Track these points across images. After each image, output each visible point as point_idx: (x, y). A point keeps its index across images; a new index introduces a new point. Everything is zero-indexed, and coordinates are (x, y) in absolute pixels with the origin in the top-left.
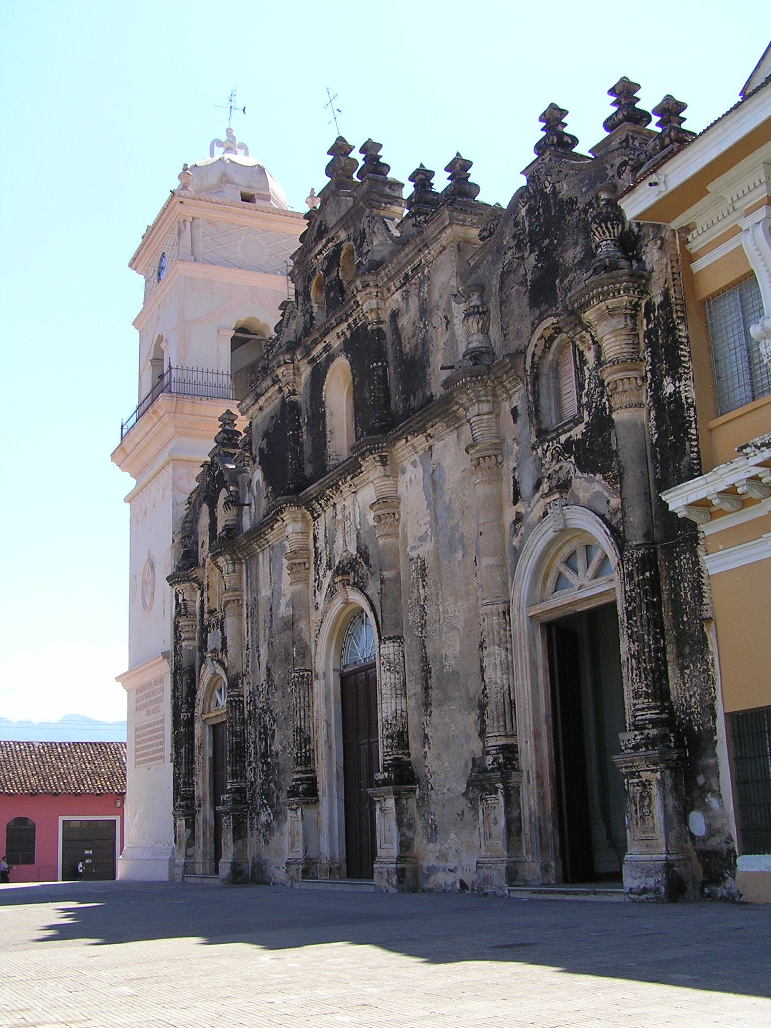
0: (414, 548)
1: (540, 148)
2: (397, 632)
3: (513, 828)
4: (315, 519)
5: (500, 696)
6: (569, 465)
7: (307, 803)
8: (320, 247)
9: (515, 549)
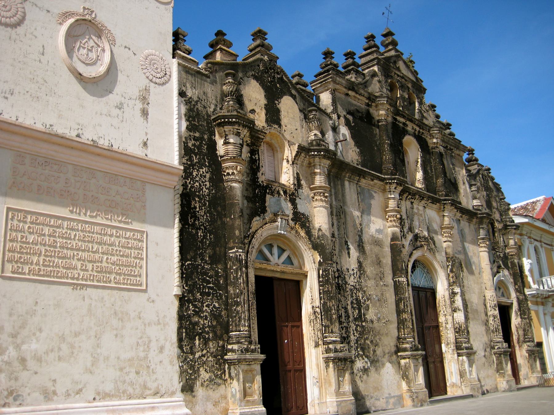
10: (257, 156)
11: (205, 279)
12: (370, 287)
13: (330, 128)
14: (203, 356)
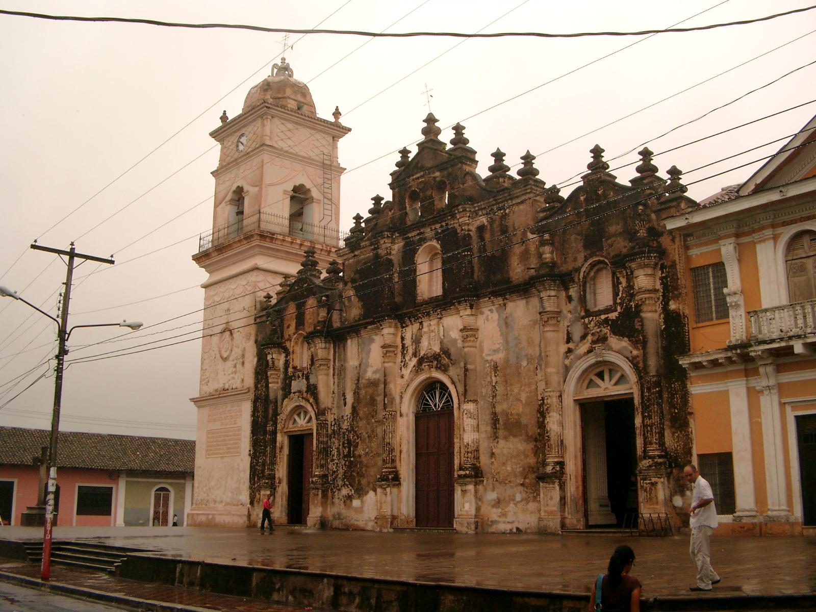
0: (487, 355)
1: (590, 166)
2: (475, 398)
3: (563, 499)
4: (403, 327)
5: (556, 437)
6: (606, 330)
7: (394, 485)
8: (418, 175)
9: (566, 366)
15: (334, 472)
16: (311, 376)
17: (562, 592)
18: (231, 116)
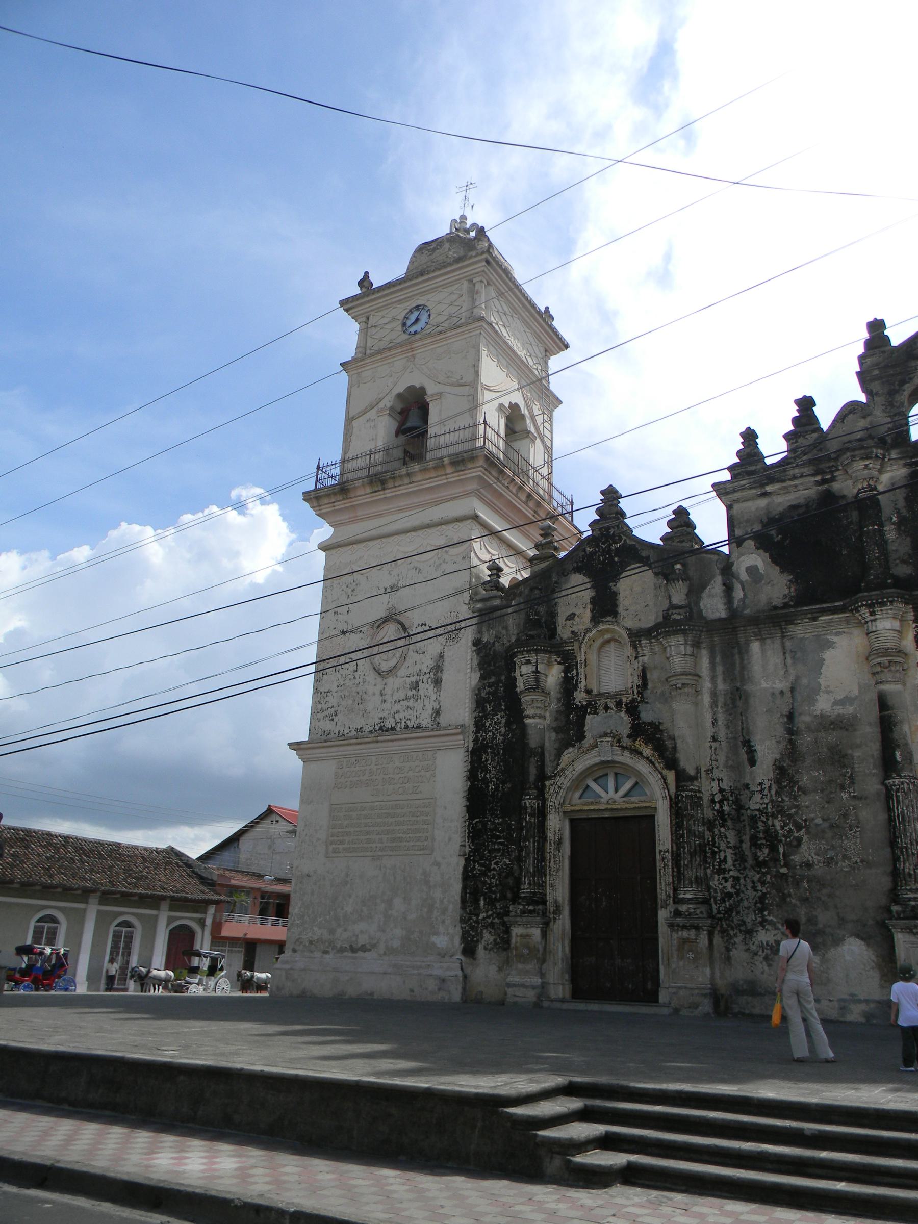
10: (574, 672)
11: (495, 835)
12: (807, 807)
13: (718, 571)
14: (488, 917)
15: (730, 895)
16: (642, 707)
17: (372, 1079)
18: (377, 281)
